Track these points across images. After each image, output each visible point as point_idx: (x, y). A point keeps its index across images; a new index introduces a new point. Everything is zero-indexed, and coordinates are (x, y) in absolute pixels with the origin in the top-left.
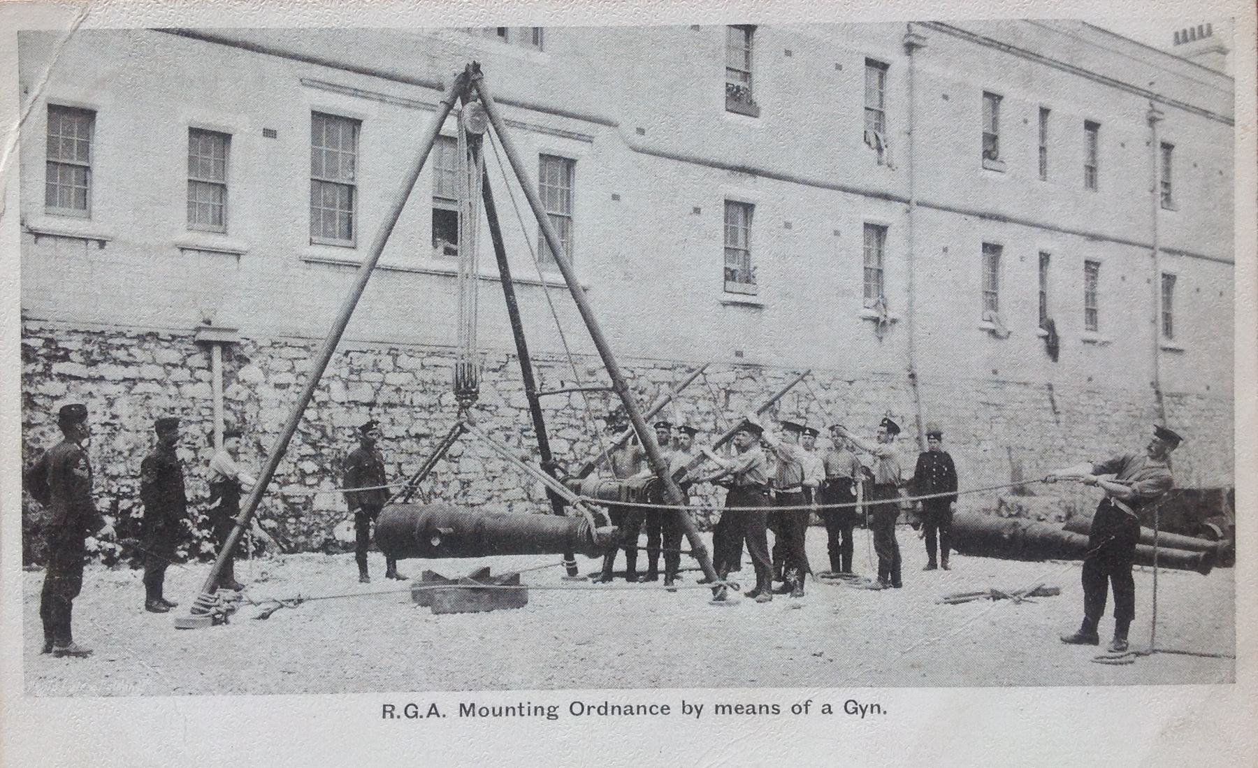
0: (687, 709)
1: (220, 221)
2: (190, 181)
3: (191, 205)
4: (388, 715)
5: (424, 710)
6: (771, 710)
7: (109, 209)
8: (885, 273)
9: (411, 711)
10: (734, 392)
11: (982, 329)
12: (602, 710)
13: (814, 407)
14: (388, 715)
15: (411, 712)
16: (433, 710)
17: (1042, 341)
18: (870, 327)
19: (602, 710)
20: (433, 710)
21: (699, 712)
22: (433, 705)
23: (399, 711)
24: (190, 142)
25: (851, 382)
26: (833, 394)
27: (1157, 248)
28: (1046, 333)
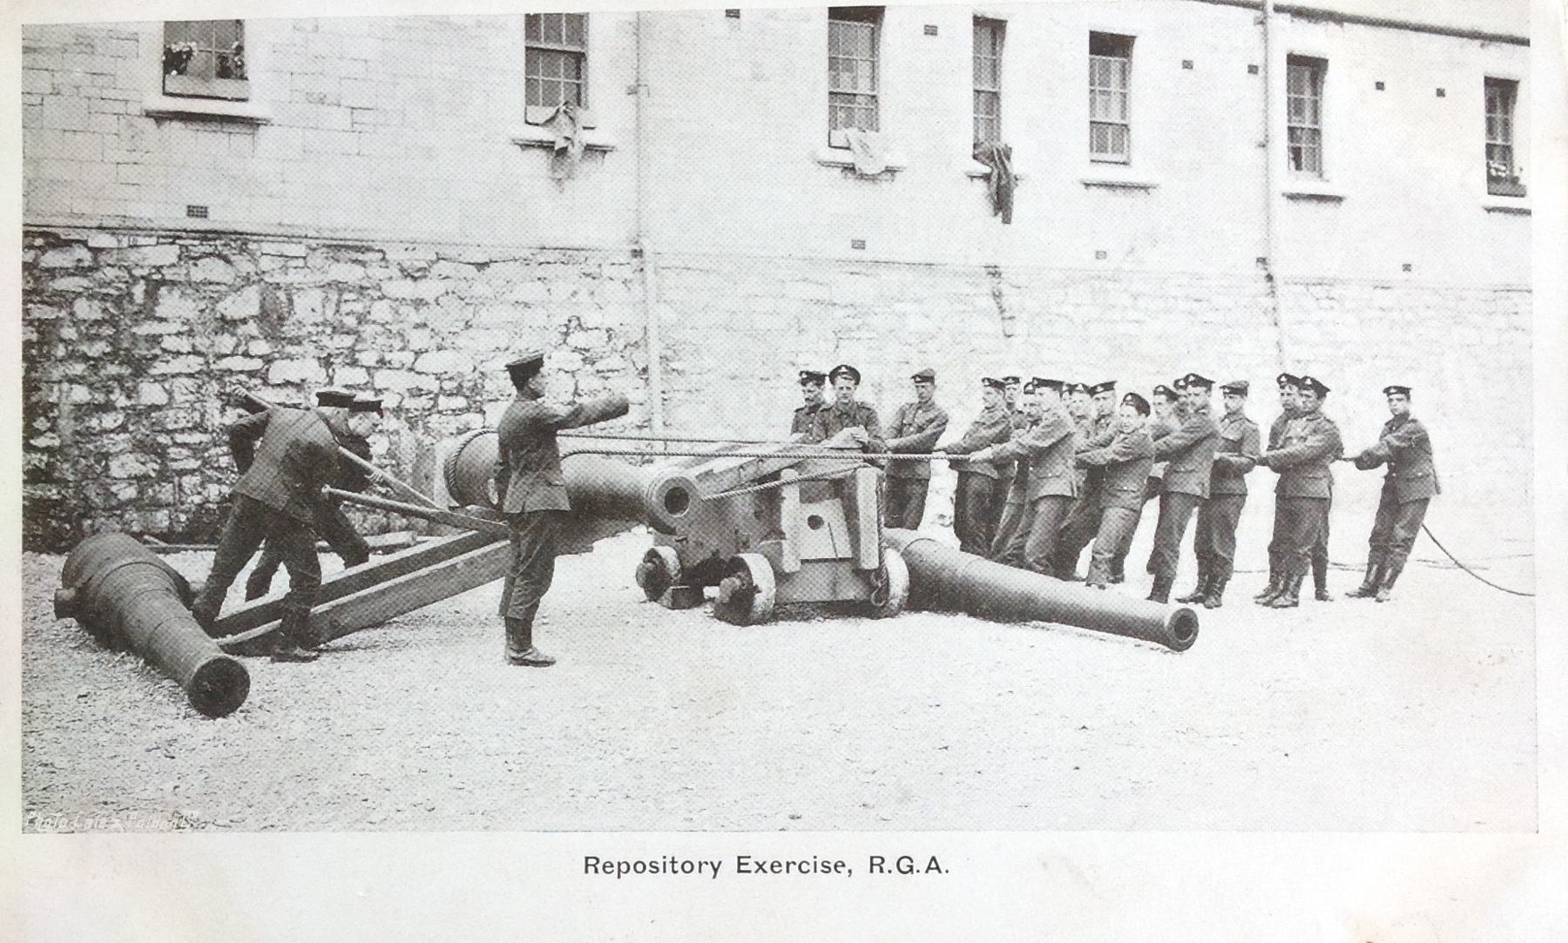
0: (906, 866)
1: (1317, 168)
2: (527, 48)
3: (530, 84)
4: (876, 869)
5: (921, 863)
6: (819, 868)
7: (894, 138)
8: (1004, 102)
9: (904, 864)
10: (163, 282)
11: (527, 146)
12: (624, 867)
13: (381, 311)
14: (876, 869)
15: (906, 866)
16: (934, 865)
17: (981, 186)
18: (540, 158)
19: (624, 867)
20: (934, 865)
21: (716, 870)
22: (933, 859)
23: (767, 867)
24: (975, 33)
25: (481, 266)
26: (428, 289)
27: (1270, 9)
28: (987, 170)
